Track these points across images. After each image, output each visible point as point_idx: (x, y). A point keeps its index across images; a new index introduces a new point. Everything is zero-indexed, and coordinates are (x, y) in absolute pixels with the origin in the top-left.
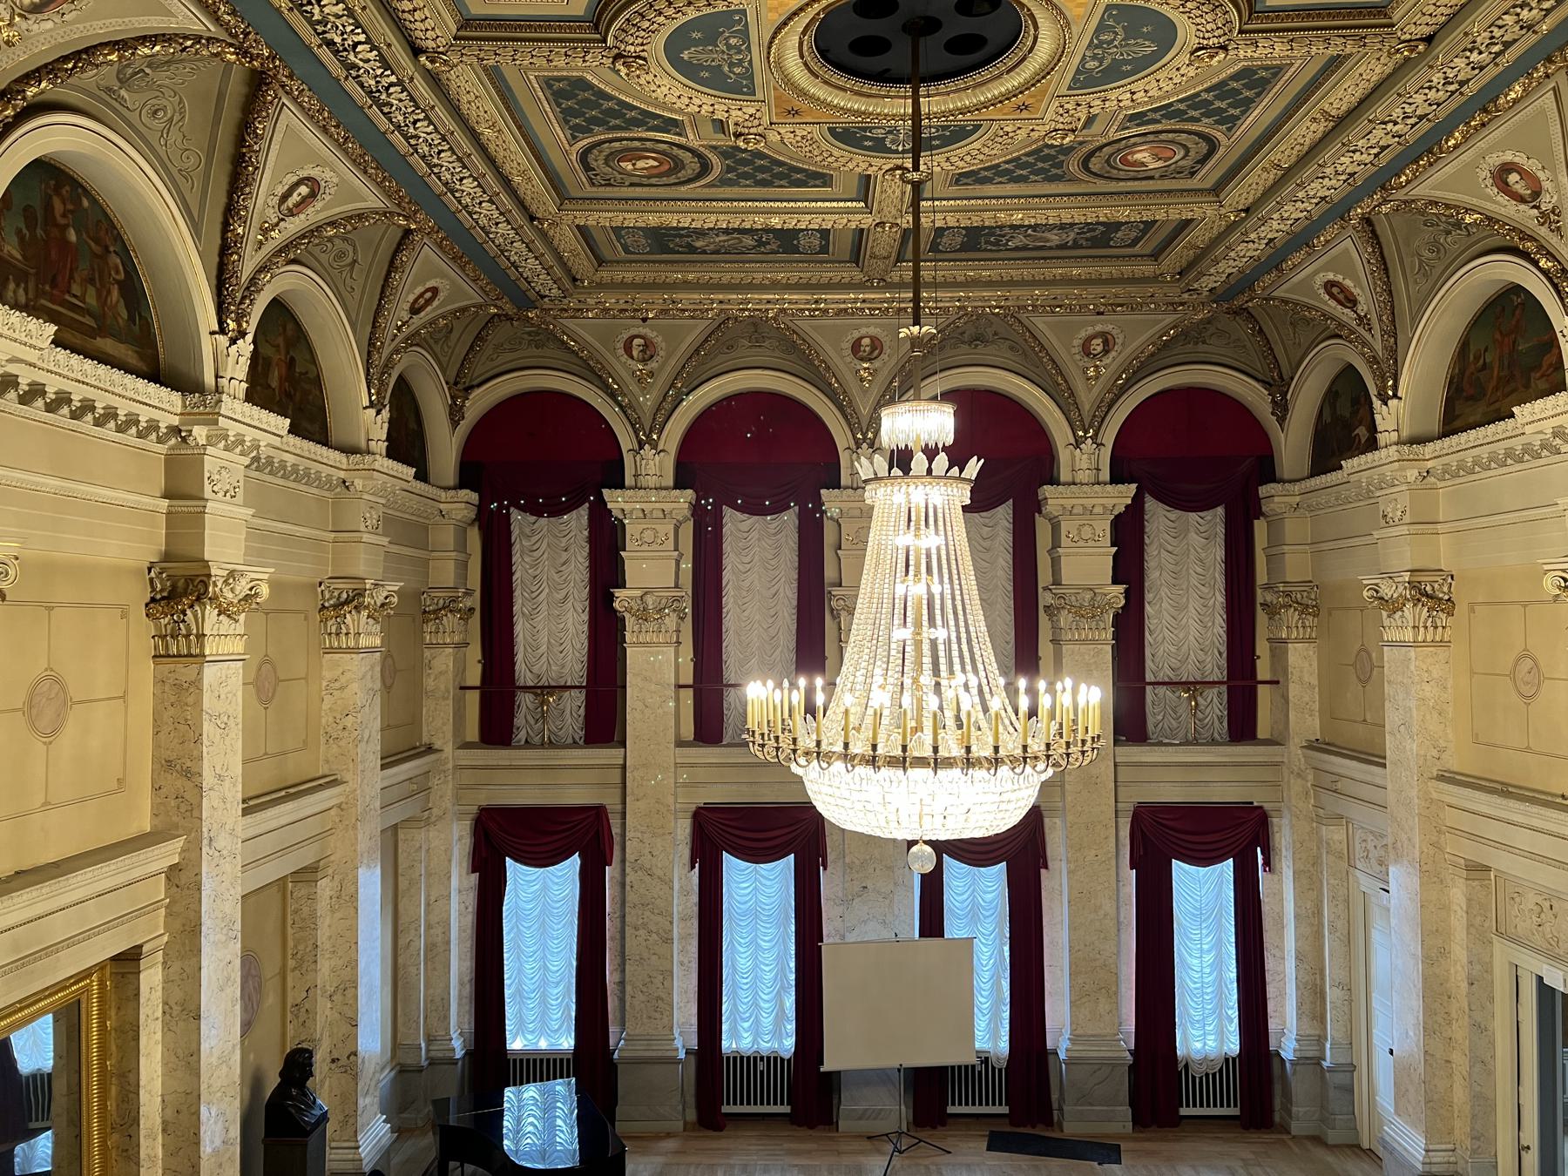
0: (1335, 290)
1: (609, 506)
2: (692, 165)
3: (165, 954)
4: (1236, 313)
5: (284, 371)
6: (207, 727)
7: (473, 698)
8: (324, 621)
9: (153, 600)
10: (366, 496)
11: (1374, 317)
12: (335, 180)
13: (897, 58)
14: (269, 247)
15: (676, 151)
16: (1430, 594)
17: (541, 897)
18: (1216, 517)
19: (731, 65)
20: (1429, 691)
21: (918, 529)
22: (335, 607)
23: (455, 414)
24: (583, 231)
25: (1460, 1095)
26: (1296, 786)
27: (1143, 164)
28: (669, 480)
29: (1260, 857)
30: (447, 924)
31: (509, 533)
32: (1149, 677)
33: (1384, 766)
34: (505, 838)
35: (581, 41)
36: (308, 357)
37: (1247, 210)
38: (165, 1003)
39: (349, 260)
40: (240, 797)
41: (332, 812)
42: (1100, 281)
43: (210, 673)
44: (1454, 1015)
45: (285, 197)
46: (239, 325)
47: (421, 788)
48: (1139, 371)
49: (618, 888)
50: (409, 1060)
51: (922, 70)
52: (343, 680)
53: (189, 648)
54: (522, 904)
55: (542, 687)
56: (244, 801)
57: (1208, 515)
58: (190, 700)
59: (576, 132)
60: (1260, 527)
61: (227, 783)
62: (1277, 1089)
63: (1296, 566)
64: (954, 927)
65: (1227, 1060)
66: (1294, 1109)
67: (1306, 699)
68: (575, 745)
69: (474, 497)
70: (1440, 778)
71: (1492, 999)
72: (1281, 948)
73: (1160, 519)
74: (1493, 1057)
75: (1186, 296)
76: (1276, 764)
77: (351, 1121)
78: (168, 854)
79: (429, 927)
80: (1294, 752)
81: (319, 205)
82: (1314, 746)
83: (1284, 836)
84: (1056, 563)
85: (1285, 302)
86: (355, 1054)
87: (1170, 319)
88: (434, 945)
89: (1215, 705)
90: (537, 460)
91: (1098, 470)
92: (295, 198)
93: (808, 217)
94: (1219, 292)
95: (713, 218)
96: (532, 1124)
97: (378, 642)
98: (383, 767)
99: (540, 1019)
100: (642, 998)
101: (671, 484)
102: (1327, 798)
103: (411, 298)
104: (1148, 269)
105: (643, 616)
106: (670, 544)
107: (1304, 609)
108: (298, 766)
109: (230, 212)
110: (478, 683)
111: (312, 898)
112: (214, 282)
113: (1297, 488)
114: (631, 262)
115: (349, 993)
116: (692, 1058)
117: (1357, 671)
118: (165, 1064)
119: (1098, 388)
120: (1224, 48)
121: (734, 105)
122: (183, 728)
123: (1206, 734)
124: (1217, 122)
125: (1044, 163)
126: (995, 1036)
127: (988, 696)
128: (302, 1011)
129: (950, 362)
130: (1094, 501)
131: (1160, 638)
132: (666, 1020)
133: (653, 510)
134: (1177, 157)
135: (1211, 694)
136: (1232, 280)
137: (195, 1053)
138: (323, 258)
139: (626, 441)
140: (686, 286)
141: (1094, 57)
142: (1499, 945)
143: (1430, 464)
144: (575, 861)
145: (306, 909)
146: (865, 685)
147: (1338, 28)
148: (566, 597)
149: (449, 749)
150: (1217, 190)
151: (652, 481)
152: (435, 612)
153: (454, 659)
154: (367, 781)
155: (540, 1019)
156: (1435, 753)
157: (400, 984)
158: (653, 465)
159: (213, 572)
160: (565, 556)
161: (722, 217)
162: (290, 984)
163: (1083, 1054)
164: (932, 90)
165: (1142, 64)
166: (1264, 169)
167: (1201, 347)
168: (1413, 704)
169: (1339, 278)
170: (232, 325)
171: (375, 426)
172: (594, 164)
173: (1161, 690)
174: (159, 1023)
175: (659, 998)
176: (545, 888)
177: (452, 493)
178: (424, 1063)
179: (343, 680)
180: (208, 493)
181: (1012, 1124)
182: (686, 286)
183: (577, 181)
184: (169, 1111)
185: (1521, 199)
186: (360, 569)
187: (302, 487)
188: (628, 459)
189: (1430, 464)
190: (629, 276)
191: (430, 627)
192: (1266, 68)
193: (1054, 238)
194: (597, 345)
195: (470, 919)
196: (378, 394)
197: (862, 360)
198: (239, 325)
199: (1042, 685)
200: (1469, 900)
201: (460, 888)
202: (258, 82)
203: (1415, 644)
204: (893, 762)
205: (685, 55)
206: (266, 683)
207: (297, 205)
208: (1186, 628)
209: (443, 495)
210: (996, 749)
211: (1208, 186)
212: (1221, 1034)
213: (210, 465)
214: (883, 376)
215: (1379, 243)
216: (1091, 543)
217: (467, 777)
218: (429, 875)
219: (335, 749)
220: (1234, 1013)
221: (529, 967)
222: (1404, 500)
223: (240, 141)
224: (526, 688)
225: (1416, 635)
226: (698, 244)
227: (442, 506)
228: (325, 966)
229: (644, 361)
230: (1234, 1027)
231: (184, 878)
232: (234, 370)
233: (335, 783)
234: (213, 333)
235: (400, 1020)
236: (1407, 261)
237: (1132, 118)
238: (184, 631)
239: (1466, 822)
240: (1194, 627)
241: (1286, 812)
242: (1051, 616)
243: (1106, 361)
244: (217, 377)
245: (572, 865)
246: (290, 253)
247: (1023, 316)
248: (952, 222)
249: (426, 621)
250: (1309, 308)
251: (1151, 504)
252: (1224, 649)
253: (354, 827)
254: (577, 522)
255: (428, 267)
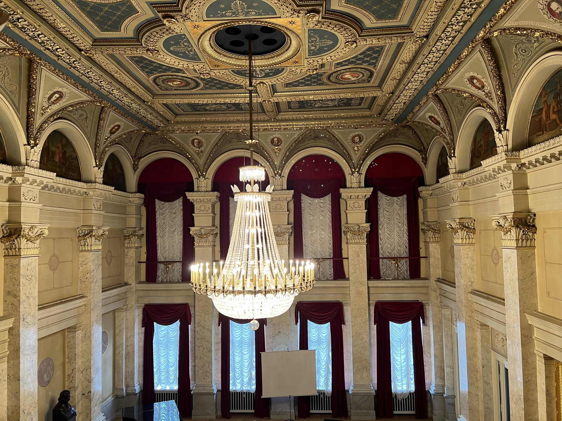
0: (433, 119)
1: (188, 198)
2: (193, 84)
3: (8, 358)
4: (404, 127)
5: (61, 155)
6: (22, 280)
7: (143, 266)
8: (80, 241)
9: (3, 237)
10: (94, 197)
11: (445, 128)
12: (69, 92)
13: (245, 48)
14: (46, 115)
15: (185, 79)
16: (467, 227)
17: (166, 335)
18: (403, 199)
19: (188, 51)
20: (468, 261)
21: (252, 210)
22: (83, 236)
23: (135, 167)
24: (166, 105)
25: (481, 408)
26: (433, 295)
27: (349, 79)
28: (210, 188)
29: (421, 320)
30: (133, 345)
31: (155, 208)
32: (381, 256)
33: (455, 287)
34: (154, 315)
35: (135, 45)
36: (72, 150)
37: (392, 93)
38: (8, 375)
39: (85, 117)
40: (37, 303)
41: (83, 307)
42: (351, 118)
43: (23, 262)
44: (479, 378)
45: (50, 98)
46: (35, 142)
47: (123, 298)
48: (372, 148)
49: (193, 333)
50: (119, 394)
51: (253, 50)
52: (86, 261)
53: (16, 253)
54: (160, 338)
55: (167, 262)
56: (39, 306)
57: (401, 198)
58: (16, 271)
59: (149, 73)
60: (420, 202)
61: (31, 299)
62: (429, 404)
63: (432, 216)
64: (311, 347)
65: (410, 394)
66: (434, 412)
67: (436, 263)
68: (178, 282)
69: (143, 196)
70: (472, 293)
71: (491, 373)
72: (430, 353)
73: (383, 199)
74: (492, 394)
75: (384, 121)
76: (427, 287)
77: (89, 415)
78: (9, 323)
79: (127, 346)
80: (432, 283)
81: (64, 100)
82: (439, 280)
83: (430, 312)
84: (425, 213)
85: (419, 123)
86: (90, 392)
87: (382, 129)
88: (129, 353)
89: (404, 266)
90: (165, 182)
91: (360, 183)
92: (54, 98)
93: (239, 99)
94: (395, 120)
95: (206, 100)
96: (163, 416)
97: (100, 248)
98: (103, 292)
99: (166, 379)
100: (201, 371)
101: (210, 190)
102: (443, 298)
103: (110, 129)
104: (368, 113)
105: (201, 236)
106: (210, 211)
107: (435, 231)
108: (67, 292)
109: (29, 104)
110: (145, 260)
111: (74, 337)
112: (25, 128)
113: (431, 188)
114: (187, 114)
115: (88, 371)
116: (220, 393)
117: (448, 254)
118: (8, 396)
119: (359, 154)
120: (355, 42)
121: (195, 64)
122: (13, 280)
123: (402, 276)
124: (369, 65)
125: (314, 80)
126: (327, 385)
127: (273, 268)
128: (71, 377)
129: (307, 146)
130: (359, 194)
131: (384, 242)
132: (209, 380)
133: (355, 195)
134: (360, 77)
135: (403, 261)
136: (398, 116)
137: (18, 392)
138: (75, 116)
139: (194, 175)
140: (207, 122)
141: (312, 46)
142: (493, 353)
143: (465, 180)
144: (178, 323)
145: (72, 342)
146: (234, 266)
147: (394, 34)
148: (175, 230)
149: (134, 284)
150: (380, 86)
151: (203, 189)
152: (128, 236)
153: (135, 251)
154: (96, 296)
155: (166, 379)
156: (470, 283)
157: (116, 367)
158: (203, 183)
159: (23, 227)
160: (174, 216)
161: (209, 100)
162: (66, 368)
163: (358, 392)
164: (256, 58)
165: (331, 48)
166: (391, 80)
167: (396, 139)
168: (462, 266)
169: (433, 115)
170: (32, 142)
171: (98, 174)
172: (159, 84)
173: (385, 260)
174: (6, 382)
175: (207, 372)
176: (168, 333)
177: (133, 194)
178: (125, 395)
179: (86, 261)
180: (22, 199)
181: (333, 417)
182: (207, 122)
183: (155, 88)
184: (10, 412)
185: (479, 89)
186: (92, 223)
187: (69, 195)
188: (195, 181)
189: (465, 180)
190: (187, 119)
191: (127, 241)
192: (378, 47)
193: (331, 104)
194: (182, 142)
195: (142, 344)
196: (99, 162)
197: (275, 146)
198: (35, 142)
199: (303, 263)
200: (482, 337)
201: (138, 332)
202: (30, 62)
203: (462, 244)
204: (250, 292)
205: (171, 49)
206: (54, 263)
207: (55, 100)
208: (393, 237)
209: (131, 195)
210: (276, 287)
211: (377, 85)
212: (408, 385)
213: (23, 190)
214: (283, 151)
215: (442, 103)
216: (358, 209)
217: (141, 294)
218: (127, 328)
219: (83, 285)
220: (413, 376)
221: (162, 360)
222: (458, 193)
223: (29, 81)
224: (161, 262)
225: (463, 241)
226: (207, 108)
227: (130, 199)
228: (79, 362)
229: (199, 147)
230: (413, 382)
231: (14, 332)
232: (33, 157)
233: (83, 297)
234: (25, 145)
235: (116, 380)
236: (453, 109)
237: (338, 64)
238: (14, 247)
239: (480, 309)
240: (396, 239)
241: (430, 304)
242: (345, 234)
243: (361, 144)
244: (27, 160)
245: (177, 324)
246: (59, 116)
247: (329, 130)
248: (294, 100)
249: (125, 239)
250: (427, 125)
251: (380, 194)
252: (407, 245)
253: (90, 313)
254: (178, 204)
255: (112, 118)
